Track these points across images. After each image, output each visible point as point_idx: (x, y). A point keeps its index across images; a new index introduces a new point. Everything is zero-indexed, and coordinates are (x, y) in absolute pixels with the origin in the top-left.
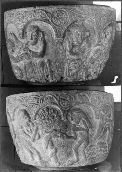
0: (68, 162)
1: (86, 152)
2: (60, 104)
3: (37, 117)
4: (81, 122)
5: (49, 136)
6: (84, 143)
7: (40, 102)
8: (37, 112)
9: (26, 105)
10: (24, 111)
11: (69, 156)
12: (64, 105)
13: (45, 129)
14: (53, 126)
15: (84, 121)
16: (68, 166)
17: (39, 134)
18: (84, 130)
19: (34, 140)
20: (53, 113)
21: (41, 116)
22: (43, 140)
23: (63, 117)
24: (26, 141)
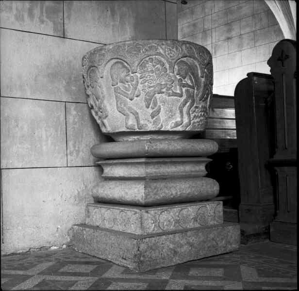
1: (191, 112)
4: (188, 77)
5: (153, 91)
12: (171, 57)
13: (148, 83)
18: (189, 86)
23: (169, 70)
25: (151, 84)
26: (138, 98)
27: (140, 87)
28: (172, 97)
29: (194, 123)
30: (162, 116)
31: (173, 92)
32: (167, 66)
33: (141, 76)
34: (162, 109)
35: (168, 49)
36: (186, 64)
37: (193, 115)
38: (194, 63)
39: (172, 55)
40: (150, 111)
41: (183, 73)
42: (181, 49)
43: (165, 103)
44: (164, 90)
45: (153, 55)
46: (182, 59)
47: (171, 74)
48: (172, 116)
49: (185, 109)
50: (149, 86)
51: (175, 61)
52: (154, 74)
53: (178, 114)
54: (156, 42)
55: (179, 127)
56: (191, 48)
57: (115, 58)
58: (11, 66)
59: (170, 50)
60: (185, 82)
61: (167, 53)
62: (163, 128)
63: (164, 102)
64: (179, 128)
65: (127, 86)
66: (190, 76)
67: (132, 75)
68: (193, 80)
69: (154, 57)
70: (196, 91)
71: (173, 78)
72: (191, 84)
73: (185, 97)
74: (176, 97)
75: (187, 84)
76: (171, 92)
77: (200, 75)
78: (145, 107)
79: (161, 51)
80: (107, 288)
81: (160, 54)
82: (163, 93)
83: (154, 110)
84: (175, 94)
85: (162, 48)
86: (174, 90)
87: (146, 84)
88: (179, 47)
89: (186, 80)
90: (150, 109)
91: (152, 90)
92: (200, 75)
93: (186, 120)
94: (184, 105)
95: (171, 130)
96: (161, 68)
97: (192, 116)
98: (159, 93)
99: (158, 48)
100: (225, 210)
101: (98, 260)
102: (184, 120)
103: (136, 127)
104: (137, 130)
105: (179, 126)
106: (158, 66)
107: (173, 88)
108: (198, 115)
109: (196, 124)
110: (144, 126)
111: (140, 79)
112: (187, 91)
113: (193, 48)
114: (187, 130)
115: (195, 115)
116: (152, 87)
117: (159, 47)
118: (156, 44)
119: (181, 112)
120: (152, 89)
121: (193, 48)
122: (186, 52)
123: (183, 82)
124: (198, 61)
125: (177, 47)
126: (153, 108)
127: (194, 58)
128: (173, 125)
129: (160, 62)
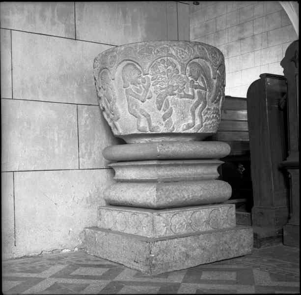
4: (200, 78)
12: (183, 58)
27: (152, 89)
28: (184, 99)
29: (205, 125)
30: (174, 118)
31: (185, 93)
32: (179, 67)
35: (180, 50)
38: (206, 64)
41: (195, 74)
44: (176, 92)
49: (197, 112)
53: (190, 117)
57: (126, 60)
59: (182, 51)
62: (175, 129)
63: (176, 104)
64: (191, 131)
71: (185, 80)
73: (196, 99)
78: (156, 109)
81: (171, 55)
87: (158, 86)
89: (198, 81)
90: (161, 111)
93: (198, 122)
94: (196, 107)
102: (196, 122)
104: (149, 132)
108: (210, 117)
112: (199, 93)
114: (199, 132)
115: (207, 118)
116: (164, 89)
123: (195, 84)
126: (165, 111)
127: (206, 59)
129: (172, 63)
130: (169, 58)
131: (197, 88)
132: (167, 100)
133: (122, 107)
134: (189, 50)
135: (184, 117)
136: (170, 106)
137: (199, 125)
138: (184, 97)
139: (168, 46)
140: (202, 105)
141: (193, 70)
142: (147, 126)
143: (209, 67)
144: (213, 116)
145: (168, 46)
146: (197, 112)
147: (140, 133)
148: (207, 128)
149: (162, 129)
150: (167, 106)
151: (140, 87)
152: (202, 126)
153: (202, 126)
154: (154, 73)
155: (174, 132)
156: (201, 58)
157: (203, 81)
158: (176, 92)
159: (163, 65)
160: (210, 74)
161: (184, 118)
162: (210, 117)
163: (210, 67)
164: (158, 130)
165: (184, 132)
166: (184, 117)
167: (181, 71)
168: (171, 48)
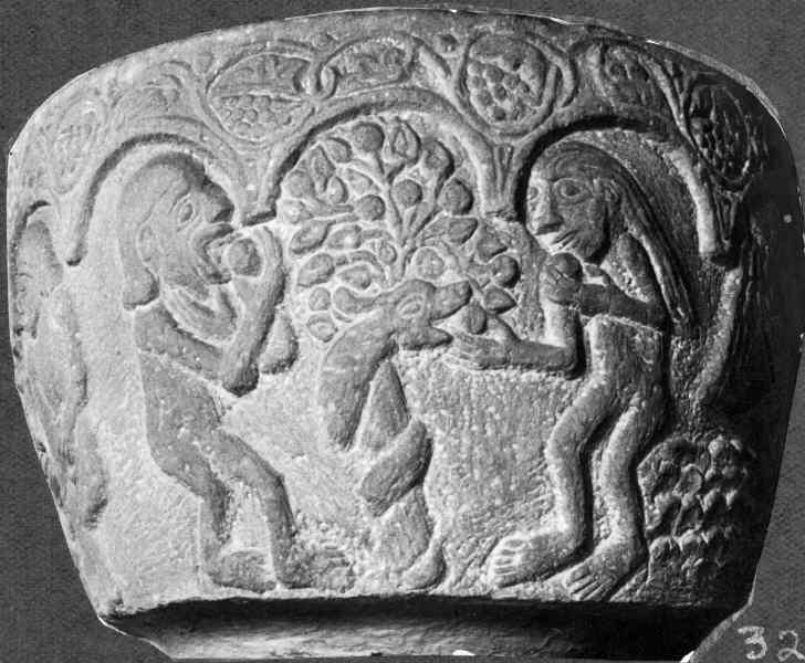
0: (505, 553)
2: (467, 105)
3: (285, 194)
4: (620, 247)
5: (379, 333)
6: (145, 640)
7: (318, 86)
8: (294, 157)
9: (204, 118)
10: (182, 164)
11: (289, 586)
12: (501, 116)
13: (346, 278)
14: (407, 259)
15: (636, 246)
16: (503, 586)
17: (290, 329)
18: (631, 308)
19: (244, 385)
20: (416, 160)
21: (318, 186)
22: (507, 33)
23: (490, 194)
24: (195, 562)
25: (365, 285)
26: (286, 379)
27: (298, 305)
28: (510, 373)
29: (669, 553)
30: (444, 501)
31: (512, 336)
32: (476, 169)
33: (298, 238)
34: (438, 448)
35: (480, 67)
36: (607, 163)
37: (659, 498)
38: (665, 167)
39: (507, 105)
40: (363, 460)
41: (583, 218)
42: (567, 74)
43: (454, 408)
44: (454, 325)
45: (380, 106)
46: (577, 136)
47: (500, 224)
48: (510, 499)
49: (606, 461)
50: (352, 296)
51: (526, 140)
52: (389, 219)
53: (558, 491)
54: (405, 27)
55: (564, 576)
56: (642, 73)
57: (147, 139)
58: (433, 289)
59: (498, 74)
60: (599, 281)
61: (474, 91)
62: (451, 577)
63: (451, 403)
64: (565, 585)
65: (213, 303)
66: (636, 246)
67: (247, 232)
68: (657, 269)
69: (387, 115)
70: (677, 346)
71: (513, 252)
72: (642, 297)
73: (599, 372)
74: (534, 375)
75: (615, 290)
76: (497, 335)
77: (705, 242)
78: (322, 435)
79: (445, 87)
80: (452, 651)
81: (430, 98)
82: (447, 341)
83: (382, 454)
84: (524, 354)
85: (441, 61)
86: (518, 329)
87: (335, 283)
88: (558, 62)
89: (605, 266)
90: (357, 448)
91: (371, 326)
92: (705, 242)
93: (614, 531)
94: (598, 432)
95: (500, 595)
96: (431, 184)
97: (654, 510)
98: (417, 347)
99: (413, 64)
100: (674, 531)
101: (691, 143)
102: (601, 528)
103: (269, 571)
104: (281, 592)
105: (562, 567)
106: (421, 172)
107: (510, 316)
108: (696, 505)
109: (692, 563)
110: (321, 562)
111: (299, 252)
112: (616, 338)
113: (657, 72)
114: (619, 596)
115: (675, 505)
116: (369, 304)
117: (425, 59)
118: (405, 35)
119: (580, 471)
120: (373, 315)
121: (657, 72)
122: (604, 91)
123: (590, 280)
124: (693, 152)
125: (541, 57)
126: (378, 447)
127: (664, 131)
128: (517, 560)
129: (425, 145)
130: (405, 115)
131: (604, 310)
132: (395, 377)
133: (119, 426)
134: (543, 76)
135: (514, 492)
136: (416, 417)
137: (619, 551)
138: (505, 363)
139: (642, 587)
140: (636, 418)
141: (572, 191)
142: (266, 549)
143: (683, 188)
144: (719, 501)
145: (642, 587)
146: (606, 461)
147: (222, 594)
148: (680, 574)
149: (373, 576)
150: (398, 406)
151: (225, 299)
152: (640, 560)
153: (640, 560)
154: (308, 202)
155: (443, 588)
156: (627, 124)
157: (639, 259)
158: (454, 325)
159: (369, 158)
160: (694, 232)
161: (519, 492)
162: (696, 505)
163: (692, 187)
164: (340, 579)
165: (511, 592)
166: (514, 492)
167: (488, 197)
168: (425, 59)
